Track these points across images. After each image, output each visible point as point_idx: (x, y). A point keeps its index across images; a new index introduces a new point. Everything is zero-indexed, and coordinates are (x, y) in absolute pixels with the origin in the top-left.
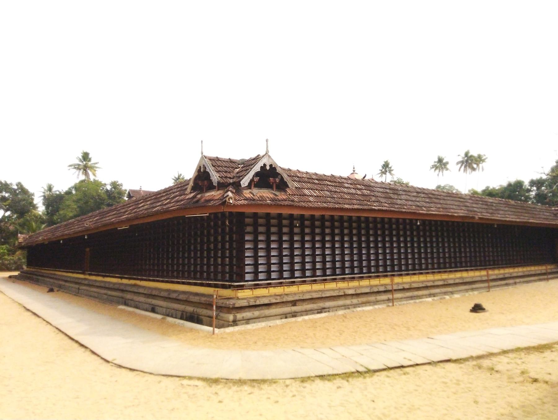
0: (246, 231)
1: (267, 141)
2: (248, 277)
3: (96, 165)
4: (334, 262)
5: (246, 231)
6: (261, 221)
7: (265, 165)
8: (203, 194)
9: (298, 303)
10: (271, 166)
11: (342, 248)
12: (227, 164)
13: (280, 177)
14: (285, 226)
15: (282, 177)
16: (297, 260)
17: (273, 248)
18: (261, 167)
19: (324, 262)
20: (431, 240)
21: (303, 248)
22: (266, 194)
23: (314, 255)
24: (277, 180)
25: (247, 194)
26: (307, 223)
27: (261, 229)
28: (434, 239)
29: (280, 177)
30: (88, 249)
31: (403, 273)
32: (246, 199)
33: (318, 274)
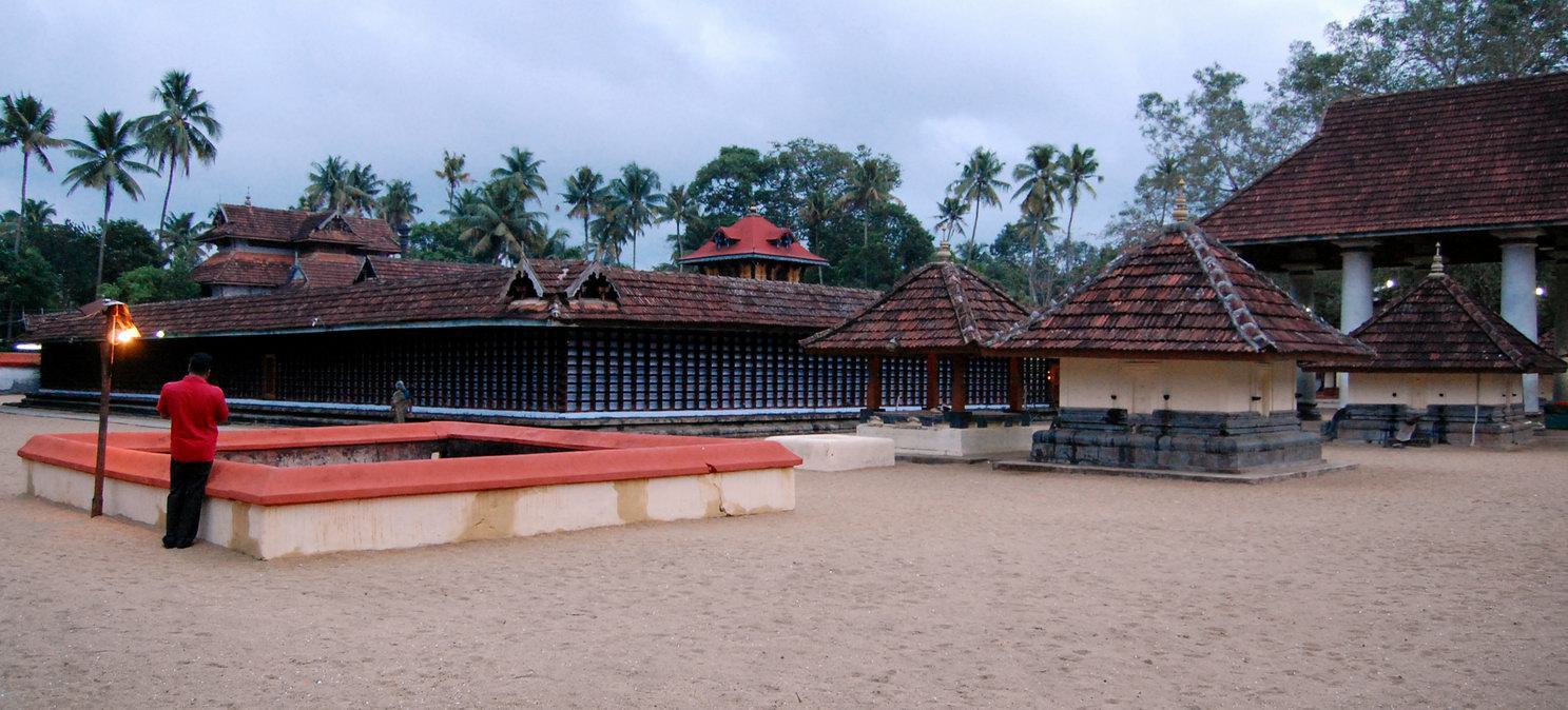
22: (594, 304)
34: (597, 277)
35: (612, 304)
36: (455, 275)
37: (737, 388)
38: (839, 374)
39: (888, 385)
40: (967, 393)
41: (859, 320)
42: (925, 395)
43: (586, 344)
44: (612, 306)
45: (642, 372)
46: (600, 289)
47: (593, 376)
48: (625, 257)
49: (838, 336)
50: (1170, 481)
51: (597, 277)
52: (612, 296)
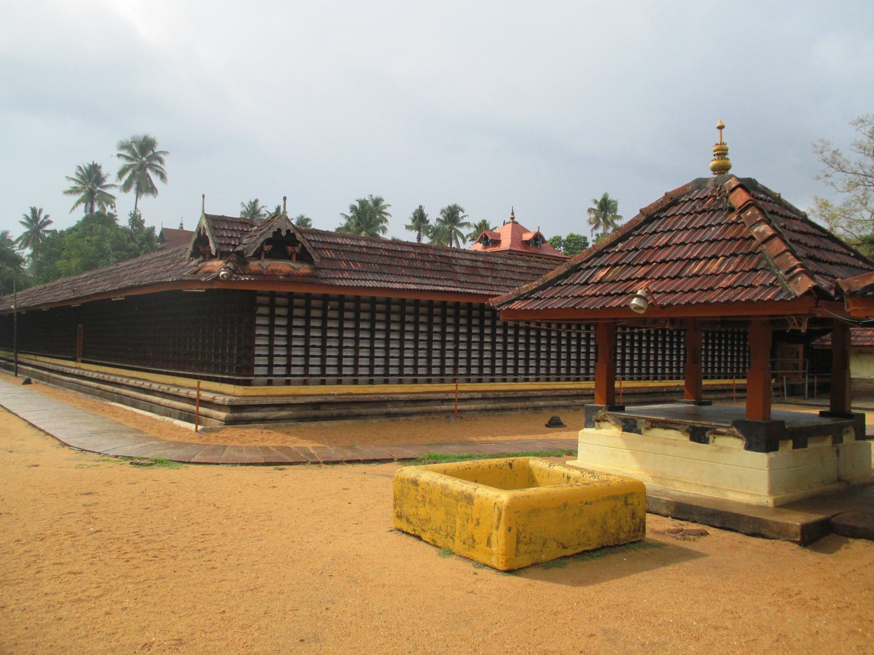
0: (257, 312)
1: (285, 199)
2: (258, 371)
3: (25, 221)
4: (578, 360)
5: (257, 312)
6: (394, 308)
7: (279, 230)
8: (204, 263)
9: (322, 407)
10: (288, 231)
11: (516, 344)
12: (391, 247)
13: (300, 245)
14: (450, 316)
15: (303, 245)
16: (532, 356)
17: (435, 341)
18: (274, 233)
19: (569, 360)
20: (739, 343)
21: (456, 342)
22: (282, 266)
23: (548, 353)
24: (297, 250)
25: (254, 265)
26: (462, 312)
27: (408, 318)
28: (723, 342)
29: (300, 245)
30: (80, 326)
31: (530, 377)
32: (252, 274)
33: (531, 372)
34: (284, 233)
35: (306, 266)
36: (827, 279)
37: (553, 363)
38: (627, 345)
39: (623, 347)
40: (615, 349)
41: (584, 266)
42: (682, 364)
43: (436, 320)
44: (304, 269)
45: (523, 349)
46: (290, 249)
47: (443, 351)
48: (619, 223)
49: (551, 292)
50: (386, 421)
51: (284, 233)
52: (304, 257)
